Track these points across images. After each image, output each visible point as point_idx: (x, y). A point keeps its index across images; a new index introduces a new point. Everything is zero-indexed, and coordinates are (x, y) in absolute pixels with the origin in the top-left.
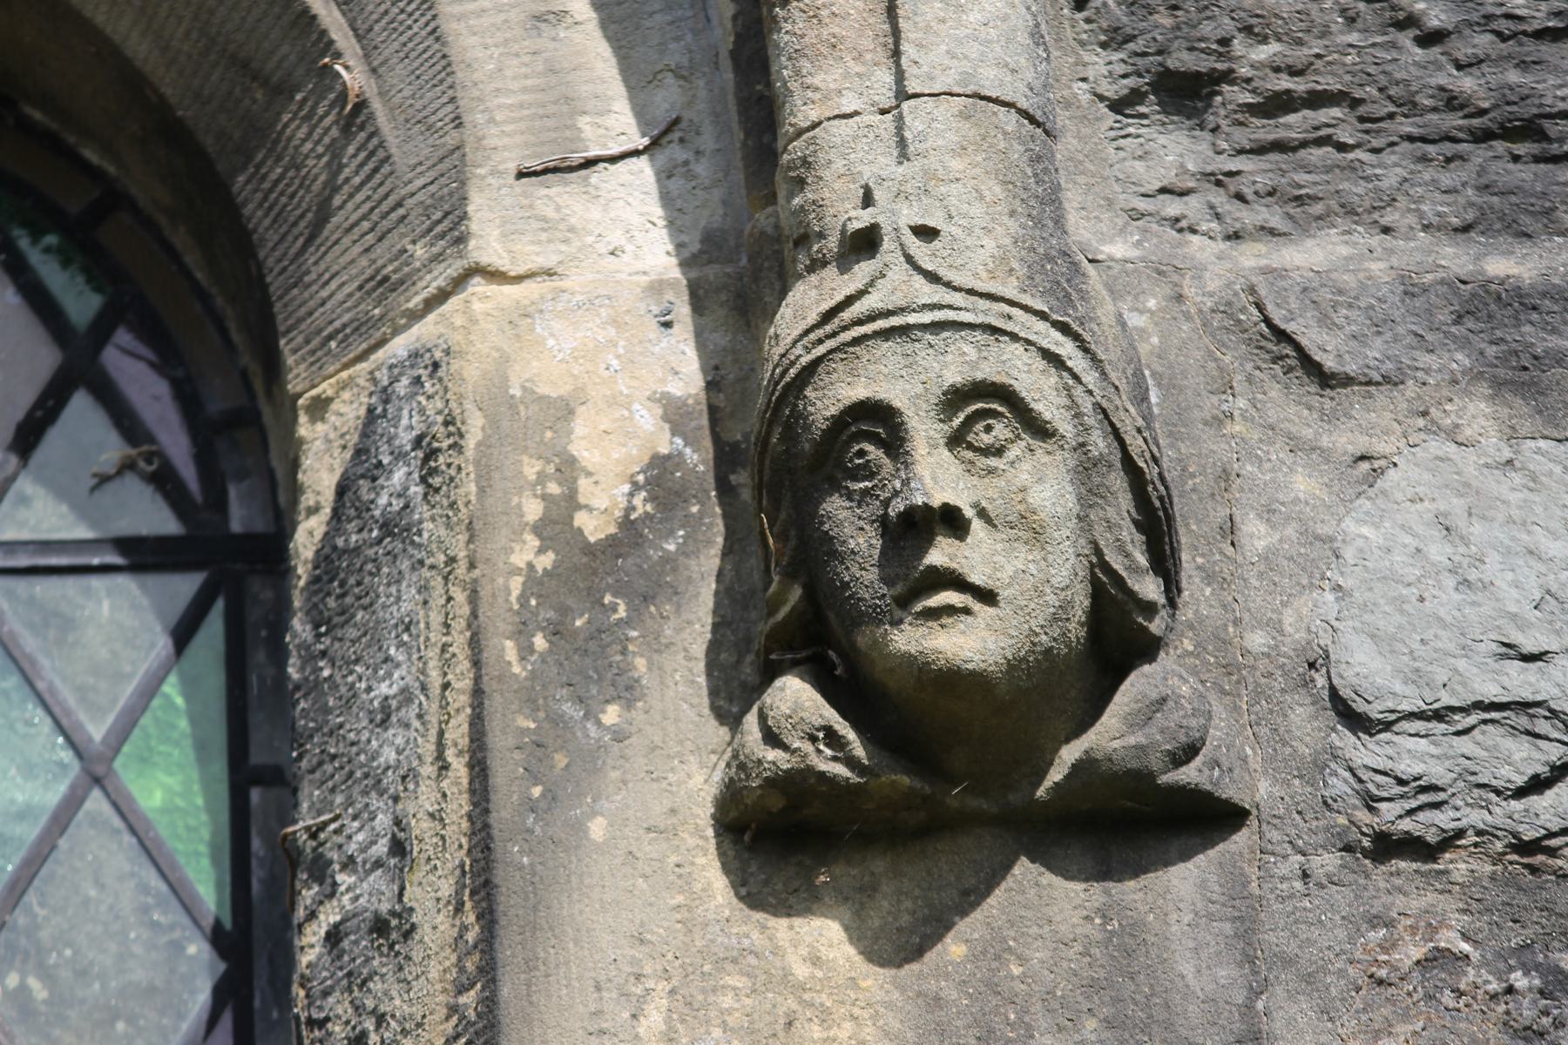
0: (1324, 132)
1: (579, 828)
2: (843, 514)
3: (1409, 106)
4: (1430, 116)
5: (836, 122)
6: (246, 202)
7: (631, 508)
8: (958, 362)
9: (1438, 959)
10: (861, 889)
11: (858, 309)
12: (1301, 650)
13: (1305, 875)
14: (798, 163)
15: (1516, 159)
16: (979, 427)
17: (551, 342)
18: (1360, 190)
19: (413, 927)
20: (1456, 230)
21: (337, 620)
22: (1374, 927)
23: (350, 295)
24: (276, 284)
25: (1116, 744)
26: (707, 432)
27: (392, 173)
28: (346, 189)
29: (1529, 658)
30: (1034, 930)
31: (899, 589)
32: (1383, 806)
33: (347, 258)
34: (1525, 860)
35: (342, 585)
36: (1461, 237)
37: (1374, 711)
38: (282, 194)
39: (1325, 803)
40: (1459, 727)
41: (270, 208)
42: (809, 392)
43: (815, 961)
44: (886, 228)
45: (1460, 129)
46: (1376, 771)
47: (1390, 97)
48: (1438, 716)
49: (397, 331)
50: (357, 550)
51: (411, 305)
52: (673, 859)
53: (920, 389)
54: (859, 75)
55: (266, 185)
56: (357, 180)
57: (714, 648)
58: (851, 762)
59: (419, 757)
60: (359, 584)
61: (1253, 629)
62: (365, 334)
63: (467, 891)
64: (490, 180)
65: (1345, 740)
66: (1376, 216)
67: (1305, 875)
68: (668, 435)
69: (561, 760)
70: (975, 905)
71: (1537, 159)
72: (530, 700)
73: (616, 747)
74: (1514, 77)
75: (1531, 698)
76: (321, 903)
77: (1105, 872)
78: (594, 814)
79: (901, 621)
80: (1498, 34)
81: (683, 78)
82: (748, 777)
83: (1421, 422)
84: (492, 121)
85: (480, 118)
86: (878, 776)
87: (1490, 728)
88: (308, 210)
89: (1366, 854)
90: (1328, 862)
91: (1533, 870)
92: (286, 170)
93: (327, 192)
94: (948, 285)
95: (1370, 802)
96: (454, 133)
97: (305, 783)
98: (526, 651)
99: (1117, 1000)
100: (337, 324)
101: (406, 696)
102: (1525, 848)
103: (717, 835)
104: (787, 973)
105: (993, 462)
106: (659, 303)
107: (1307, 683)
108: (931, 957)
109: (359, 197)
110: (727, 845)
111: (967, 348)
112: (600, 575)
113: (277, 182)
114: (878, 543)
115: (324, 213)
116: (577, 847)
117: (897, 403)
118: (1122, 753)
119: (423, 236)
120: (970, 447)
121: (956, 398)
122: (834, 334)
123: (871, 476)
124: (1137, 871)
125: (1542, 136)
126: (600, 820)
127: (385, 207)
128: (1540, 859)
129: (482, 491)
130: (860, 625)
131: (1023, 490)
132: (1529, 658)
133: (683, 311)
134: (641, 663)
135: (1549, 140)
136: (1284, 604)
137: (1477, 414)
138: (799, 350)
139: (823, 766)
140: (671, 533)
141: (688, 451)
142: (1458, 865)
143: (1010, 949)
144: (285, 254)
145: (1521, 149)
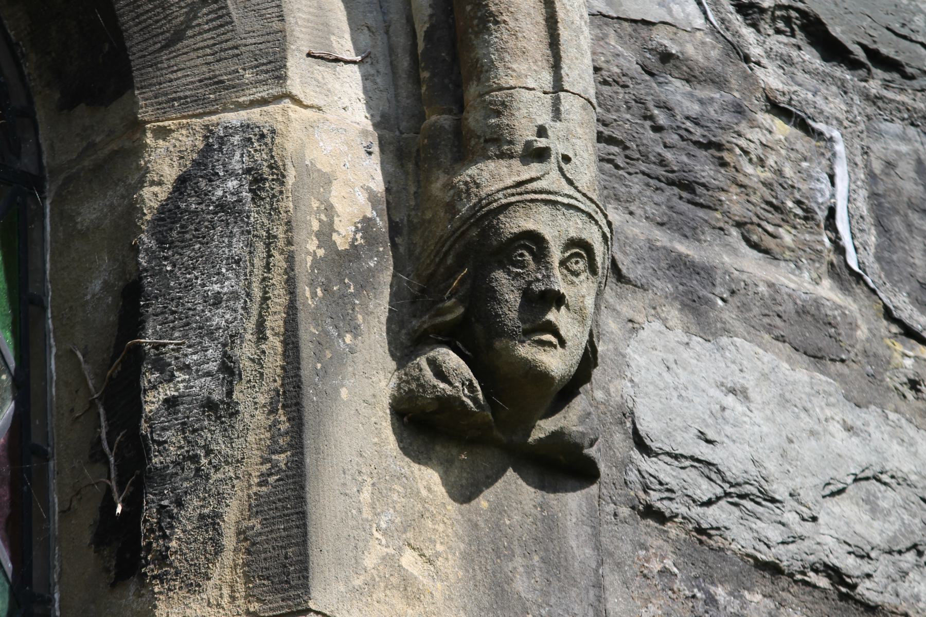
0: (611, 157)
1: (336, 390)
2: (504, 281)
3: (645, 157)
4: (652, 165)
5: (523, 90)
6: (122, 15)
7: (355, 239)
8: (575, 227)
9: (664, 572)
10: (447, 461)
11: (530, 186)
12: (620, 406)
13: (615, 515)
14: (499, 103)
15: (681, 198)
16: (574, 260)
17: (321, 144)
18: (622, 190)
19: (237, 412)
20: (658, 223)
21: (177, 243)
22: (641, 549)
23: (192, 83)
24: (137, 62)
25: (574, 428)
26: (386, 213)
27: (232, 31)
28: (197, 29)
29: (709, 442)
30: (514, 505)
31: (527, 326)
32: (651, 492)
33: (192, 63)
34: (699, 537)
35: (182, 227)
36: (659, 227)
37: (654, 446)
38: (150, 18)
39: (626, 483)
40: (683, 465)
41: (140, 23)
42: (501, 217)
43: (429, 490)
44: (553, 152)
45: (663, 176)
46: (651, 475)
47: (639, 151)
48: (676, 457)
49: (225, 110)
50: (196, 212)
51: (241, 100)
52: (373, 419)
53: (557, 233)
54: (535, 71)
55: (140, 11)
56: (206, 27)
57: (389, 320)
58: (475, 400)
59: (245, 329)
60: (196, 230)
61: (597, 389)
62: (198, 104)
63: (280, 405)
64: (296, 53)
65: (636, 455)
66: (628, 205)
67: (615, 515)
68: (370, 209)
69: (329, 354)
70: (492, 484)
71: (689, 202)
72: (316, 317)
73: (350, 356)
74: (685, 159)
75: (712, 461)
76: (161, 383)
77: (542, 486)
78: (343, 386)
79: (524, 342)
80: (681, 136)
81: (373, 33)
82: (424, 392)
83: (653, 312)
84: (296, 23)
85: (292, 20)
86: (484, 411)
87: (693, 469)
88: (168, 31)
89: (639, 512)
90: (625, 511)
91: (701, 542)
92: (156, 7)
93: (183, 27)
94: (576, 188)
95: (646, 489)
96: (279, 24)
97: (151, 320)
98: (314, 295)
99: (546, 550)
100: (182, 94)
101: (235, 296)
102: (700, 530)
103: (391, 414)
104: (419, 492)
105: (574, 279)
106: (366, 142)
107: (622, 423)
108: (474, 503)
109: (205, 36)
110: (395, 421)
111: (579, 221)
112: (342, 263)
113: (147, 11)
114: (519, 300)
115: (178, 36)
116: (336, 400)
117: (547, 237)
118: (576, 433)
119: (252, 68)
120: (567, 268)
121: (573, 243)
122: (521, 194)
123: (523, 267)
124: (555, 490)
125: (693, 191)
126: (344, 389)
127: (224, 46)
128: (704, 538)
129: (295, 208)
130: (501, 337)
131: (584, 296)
132: (709, 442)
133: (376, 149)
134: (360, 317)
135: (696, 194)
136: (610, 381)
137: (673, 314)
138: (500, 195)
139: (465, 399)
140: (371, 258)
141: (378, 219)
142: (672, 530)
143: (505, 511)
144: (146, 49)
145: (685, 195)
